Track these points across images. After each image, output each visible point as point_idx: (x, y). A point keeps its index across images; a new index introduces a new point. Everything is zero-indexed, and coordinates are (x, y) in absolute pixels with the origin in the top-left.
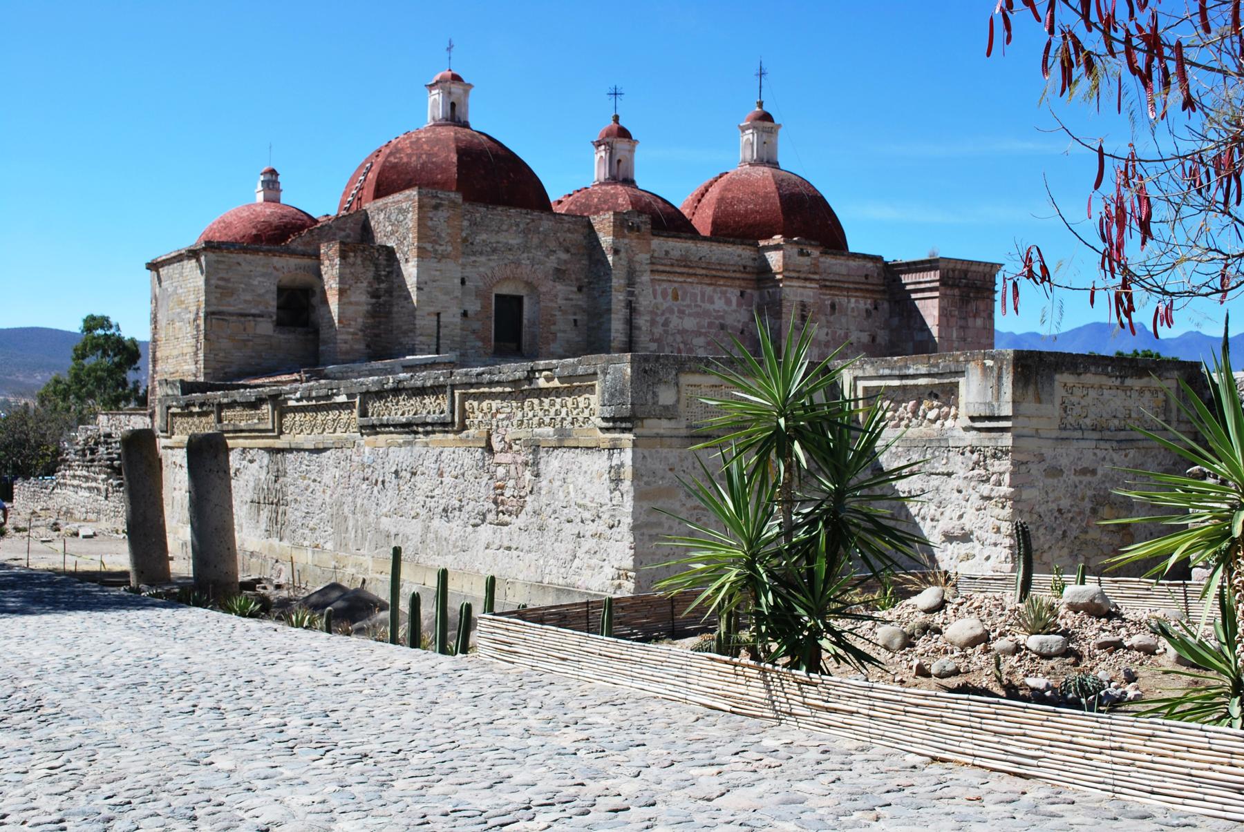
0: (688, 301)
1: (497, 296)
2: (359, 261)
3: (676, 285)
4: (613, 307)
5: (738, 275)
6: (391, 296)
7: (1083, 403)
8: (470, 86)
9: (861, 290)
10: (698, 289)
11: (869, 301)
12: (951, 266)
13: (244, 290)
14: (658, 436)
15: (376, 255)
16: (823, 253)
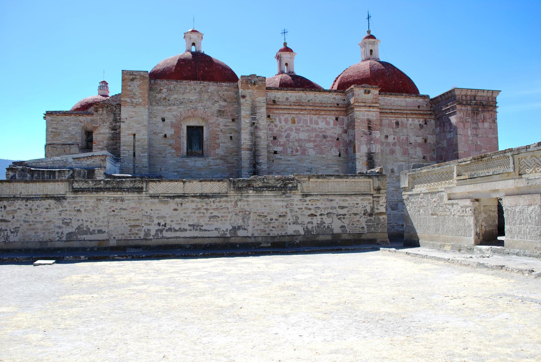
0: (301, 124)
1: (188, 127)
2: (105, 112)
3: (294, 116)
5: (334, 109)
9: (415, 114)
10: (308, 117)
11: (421, 120)
12: (464, 93)
13: (65, 133)
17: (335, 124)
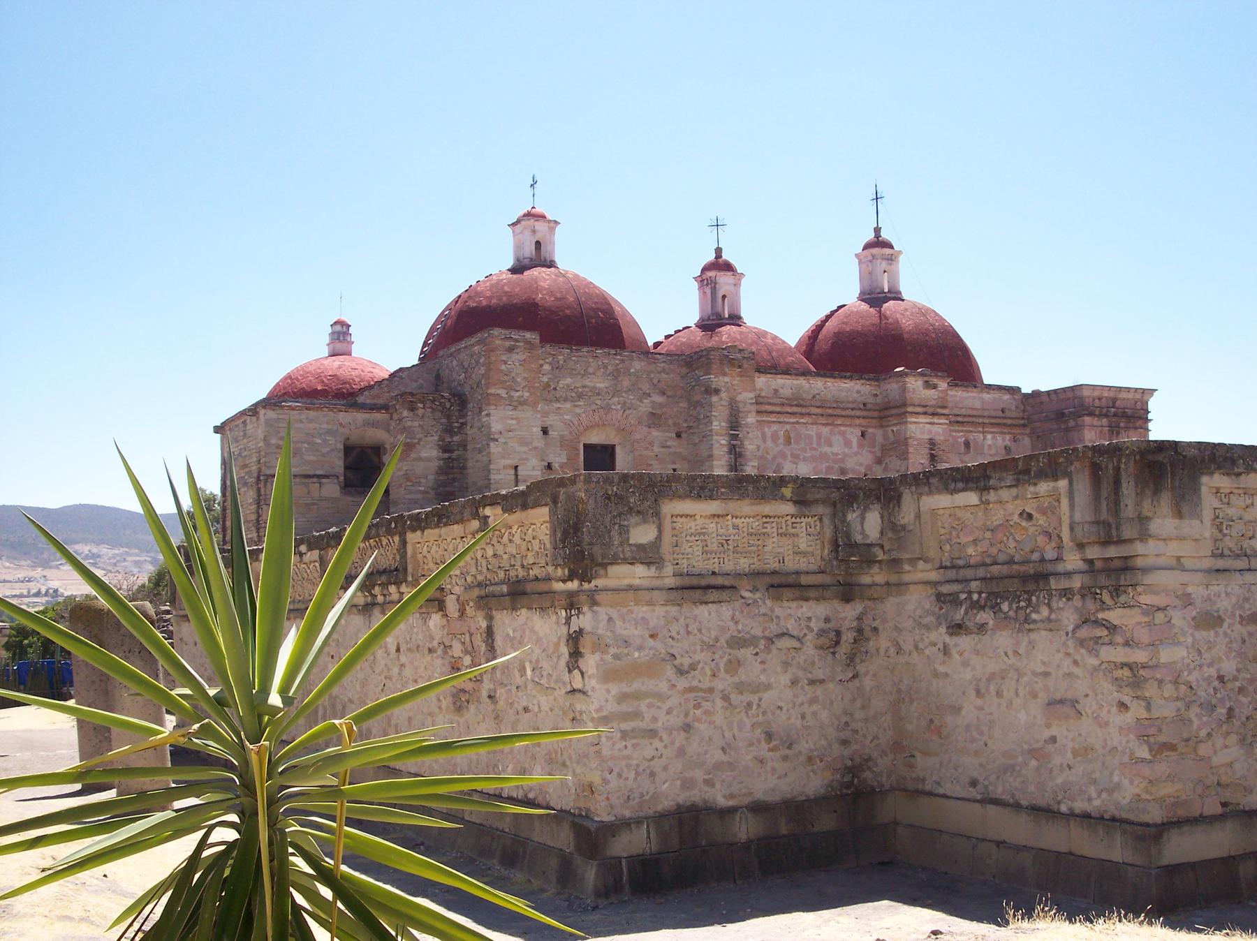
3: (788, 427)
4: (715, 452)
5: (858, 413)
6: (465, 449)
7: (1247, 517)
8: (556, 223)
9: (998, 425)
10: (812, 431)
12: (1097, 394)
14: (631, 588)
15: (448, 405)
16: (952, 385)
17: (861, 446)
